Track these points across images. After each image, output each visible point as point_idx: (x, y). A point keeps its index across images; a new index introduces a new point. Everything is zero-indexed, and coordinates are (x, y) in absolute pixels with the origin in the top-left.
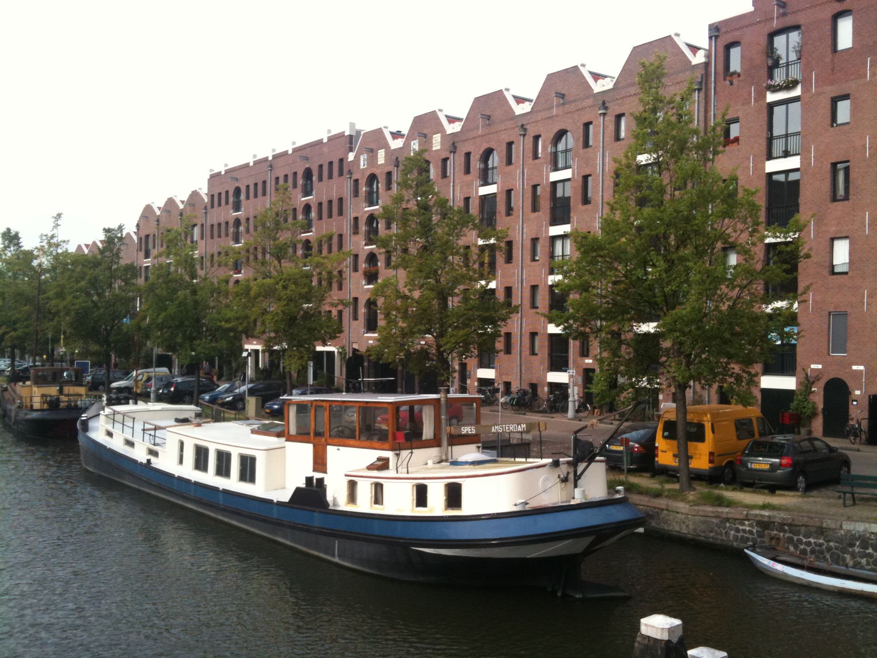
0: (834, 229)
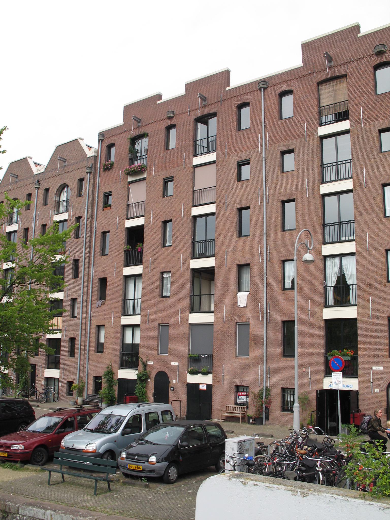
0: (162, 266)
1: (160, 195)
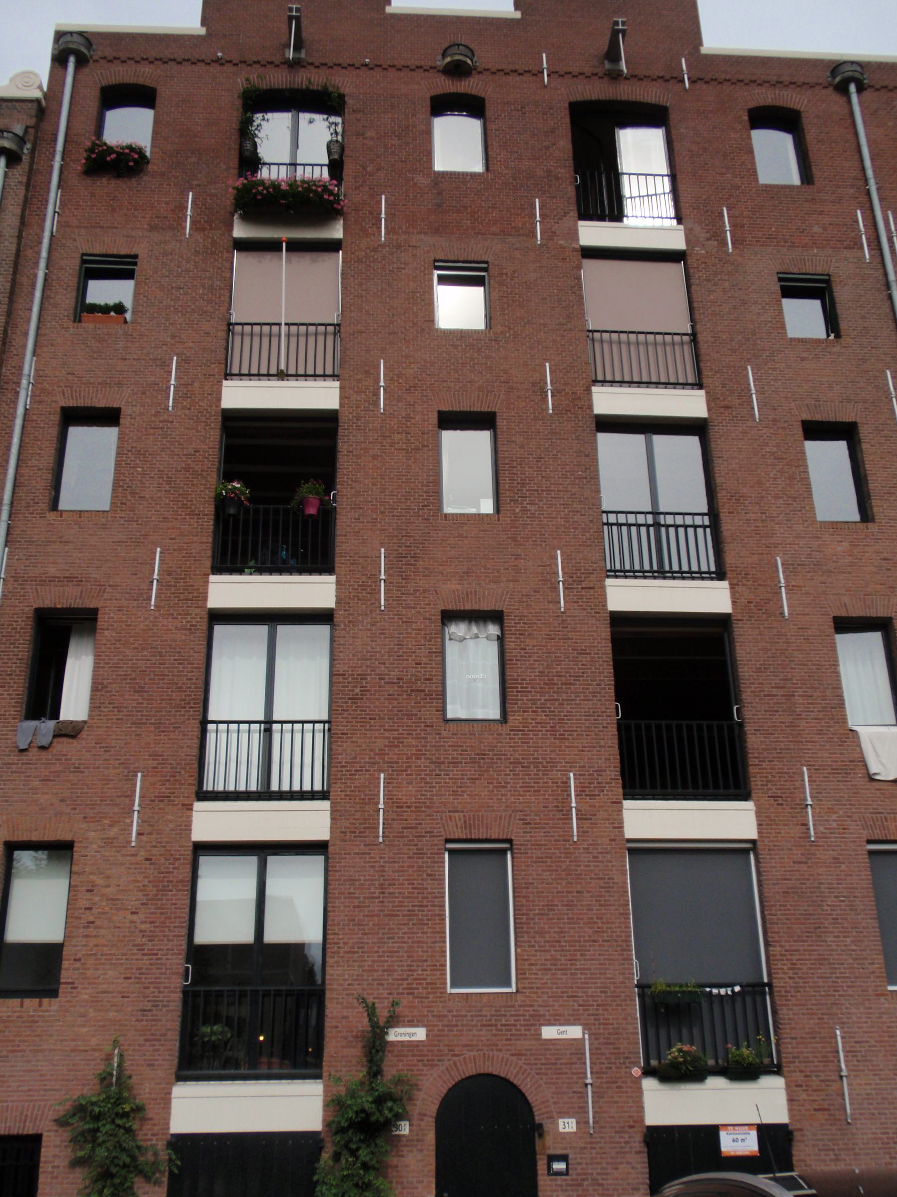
0: (453, 585)
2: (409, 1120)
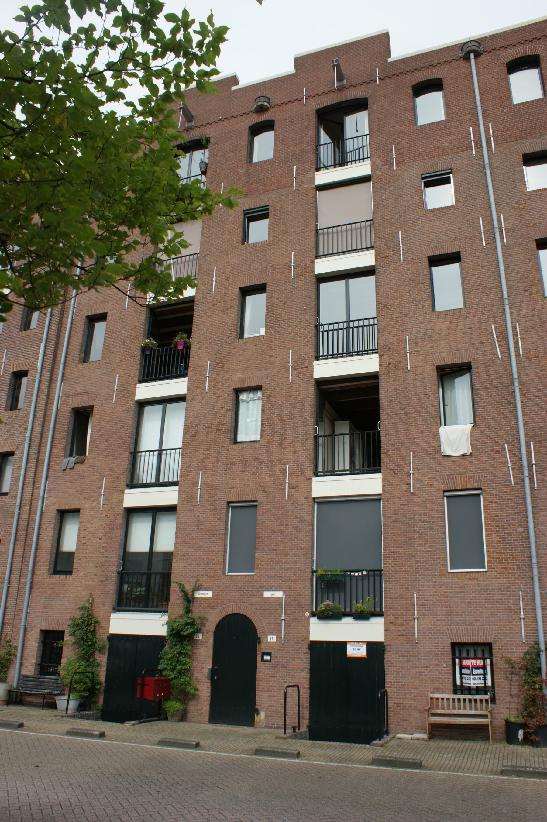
0: (240, 375)
1: (235, 239)
2: (202, 633)
